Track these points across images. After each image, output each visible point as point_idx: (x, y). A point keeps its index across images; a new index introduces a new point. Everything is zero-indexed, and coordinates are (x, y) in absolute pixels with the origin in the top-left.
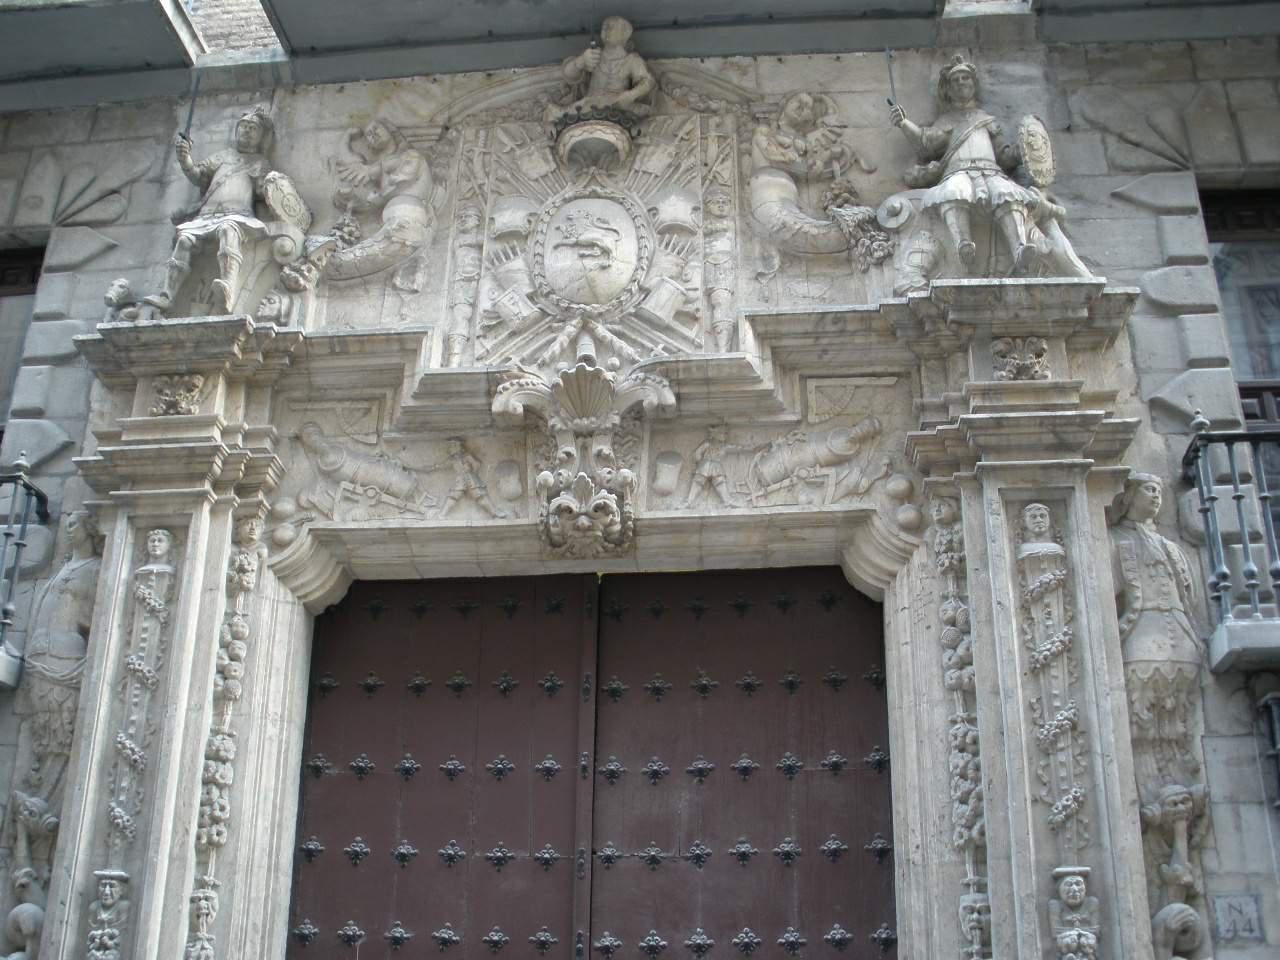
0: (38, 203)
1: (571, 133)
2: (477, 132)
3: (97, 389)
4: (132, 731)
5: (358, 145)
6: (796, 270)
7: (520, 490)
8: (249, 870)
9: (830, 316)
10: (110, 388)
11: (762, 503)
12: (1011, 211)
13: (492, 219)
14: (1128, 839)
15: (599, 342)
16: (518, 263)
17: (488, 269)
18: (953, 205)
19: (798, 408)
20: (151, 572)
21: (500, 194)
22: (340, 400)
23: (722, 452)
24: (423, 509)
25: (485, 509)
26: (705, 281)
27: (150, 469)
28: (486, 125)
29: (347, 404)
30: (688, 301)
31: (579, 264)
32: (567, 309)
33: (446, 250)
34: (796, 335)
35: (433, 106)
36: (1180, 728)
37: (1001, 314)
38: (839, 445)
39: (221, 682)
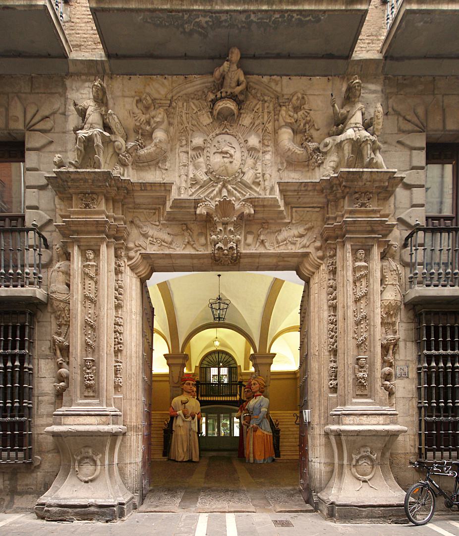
0: (16, 119)
1: (218, 104)
2: (183, 104)
3: (57, 200)
4: (90, 316)
5: (140, 105)
6: (291, 168)
7: (205, 242)
8: (131, 357)
9: (304, 184)
10: (61, 199)
11: (277, 249)
12: (367, 144)
13: (191, 141)
14: (379, 350)
15: (228, 191)
16: (201, 160)
17: (191, 162)
18: (348, 141)
19: (290, 218)
20: (89, 265)
21: (193, 131)
22: (145, 209)
23: (266, 232)
24: (175, 248)
25: (195, 248)
26: (263, 170)
27: (83, 228)
28: (187, 101)
29: (148, 210)
30: (257, 178)
31: (222, 160)
32: (218, 178)
33: (176, 154)
34: (291, 191)
35: (166, 90)
36: (394, 320)
37: (360, 183)
38: (301, 230)
39: (116, 301)
